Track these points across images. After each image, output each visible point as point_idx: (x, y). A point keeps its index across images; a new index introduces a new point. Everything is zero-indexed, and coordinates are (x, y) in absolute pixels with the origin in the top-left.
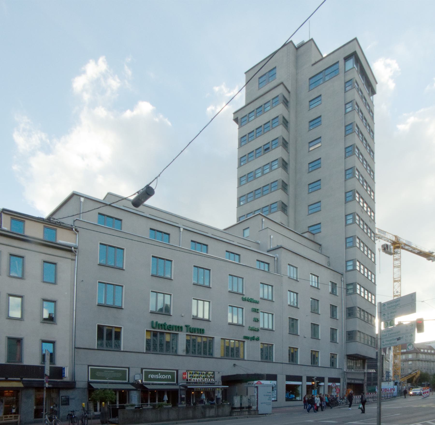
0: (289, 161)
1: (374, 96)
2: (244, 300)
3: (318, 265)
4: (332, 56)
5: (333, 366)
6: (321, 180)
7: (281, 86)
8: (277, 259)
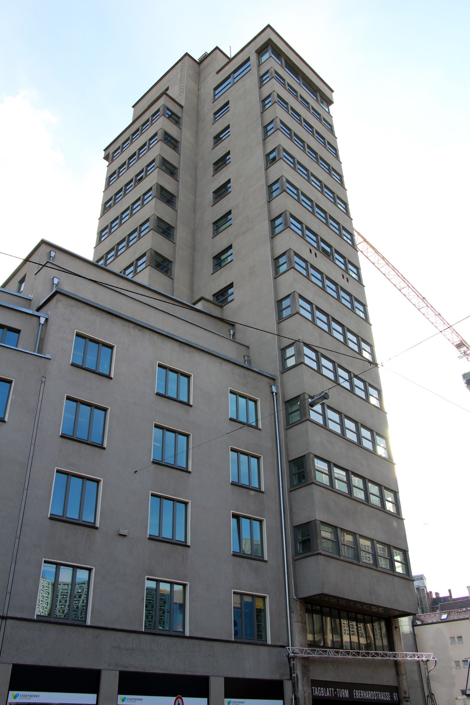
3: (187, 348)
8: (47, 319)
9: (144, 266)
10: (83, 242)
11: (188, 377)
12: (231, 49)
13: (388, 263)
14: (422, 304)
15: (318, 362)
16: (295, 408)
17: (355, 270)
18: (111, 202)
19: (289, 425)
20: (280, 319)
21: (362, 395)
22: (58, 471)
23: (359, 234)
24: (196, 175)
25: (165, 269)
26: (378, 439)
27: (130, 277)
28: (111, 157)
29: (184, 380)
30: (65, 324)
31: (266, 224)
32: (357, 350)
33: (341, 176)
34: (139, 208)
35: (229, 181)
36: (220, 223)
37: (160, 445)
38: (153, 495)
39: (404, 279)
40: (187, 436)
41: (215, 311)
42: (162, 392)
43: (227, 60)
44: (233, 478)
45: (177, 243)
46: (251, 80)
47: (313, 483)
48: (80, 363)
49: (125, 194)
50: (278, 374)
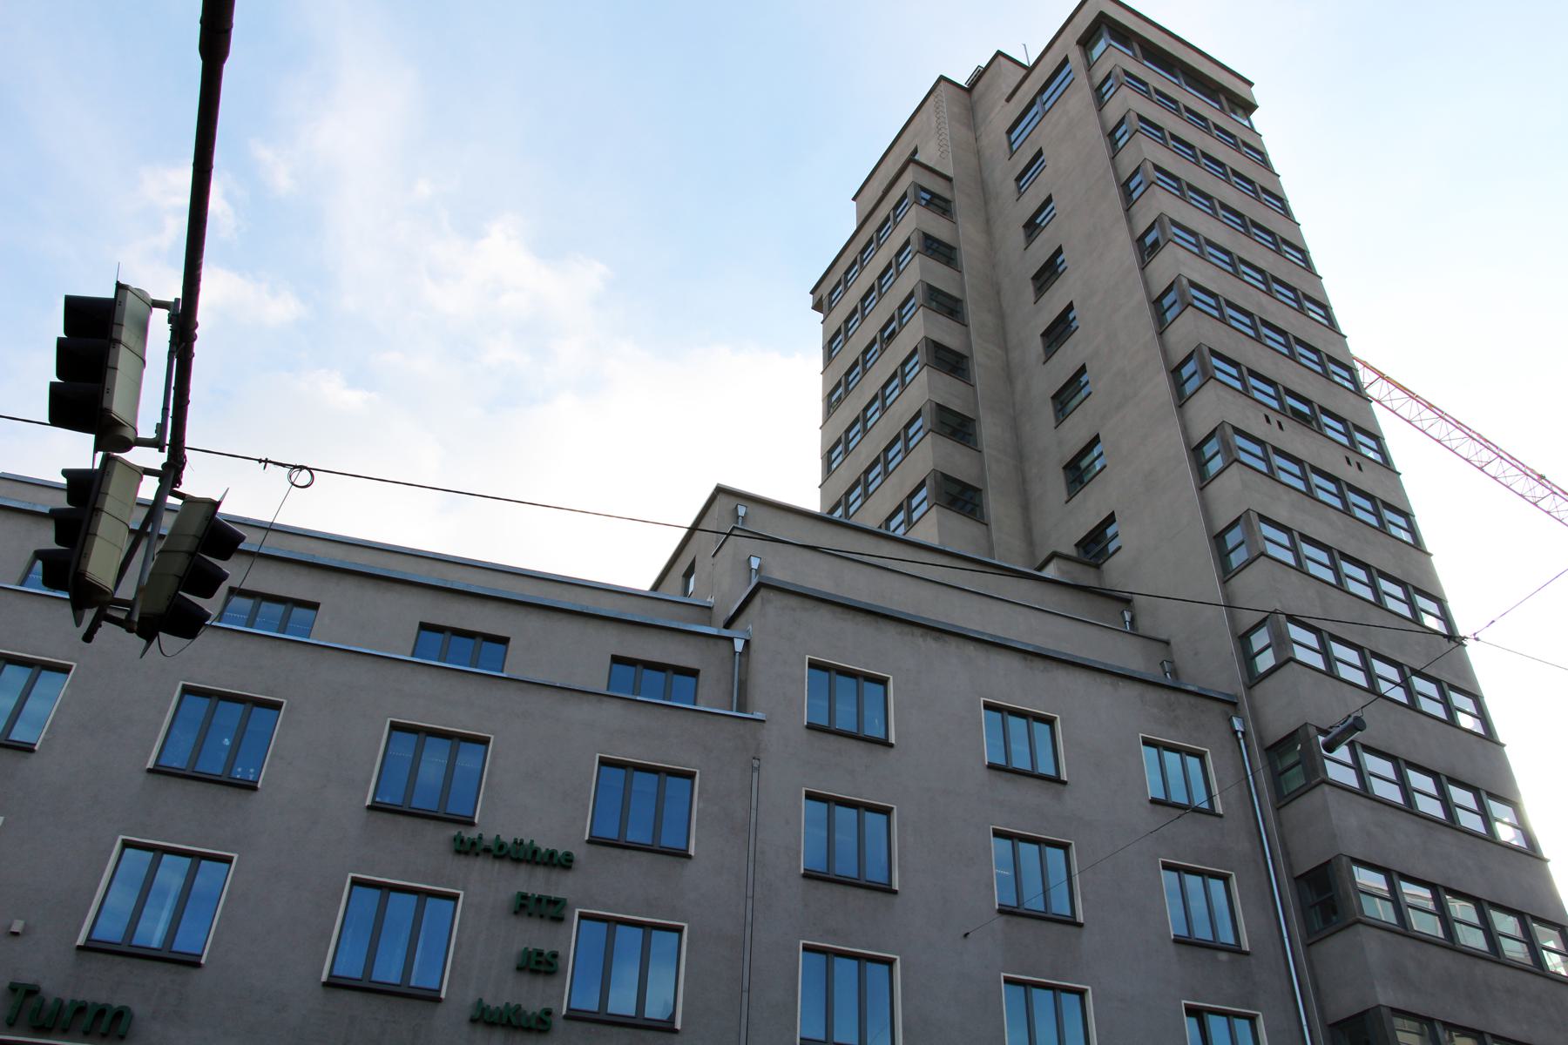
0: (969, 345)
1: (1255, 117)
2: (466, 848)
3: (1039, 664)
8: (747, 643)
9: (924, 506)
10: (794, 476)
11: (1050, 721)
12: (1028, 45)
13: (1442, 415)
14: (1540, 491)
15: (1325, 652)
16: (1291, 759)
17: (1372, 444)
18: (840, 390)
19: (1283, 799)
20: (1227, 573)
21: (1439, 711)
22: (806, 948)
23: (1365, 365)
24: (1001, 307)
25: (969, 507)
26: (1495, 807)
27: (900, 532)
28: (825, 303)
29: (1041, 730)
30: (784, 647)
31: (1163, 382)
32: (1409, 615)
33: (1303, 252)
34: (897, 392)
35: (1070, 307)
36: (1067, 396)
37: (1009, 873)
38: (1008, 981)
39: (1486, 443)
40: (1065, 847)
41: (1086, 577)
42: (1001, 761)
43: (1024, 72)
44: (1176, 927)
45: (985, 450)
46: (1078, 99)
47: (1359, 922)
48: (824, 722)
49: (865, 371)
50: (1240, 690)
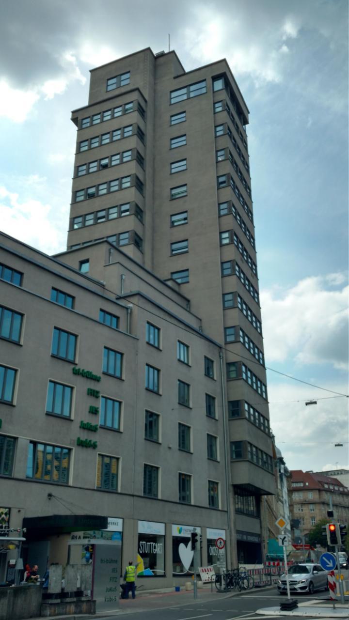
0: (145, 179)
1: (247, 126)
2: (76, 372)
4: (197, 73)
5: (213, 504)
6: (189, 270)
7: (136, 93)
